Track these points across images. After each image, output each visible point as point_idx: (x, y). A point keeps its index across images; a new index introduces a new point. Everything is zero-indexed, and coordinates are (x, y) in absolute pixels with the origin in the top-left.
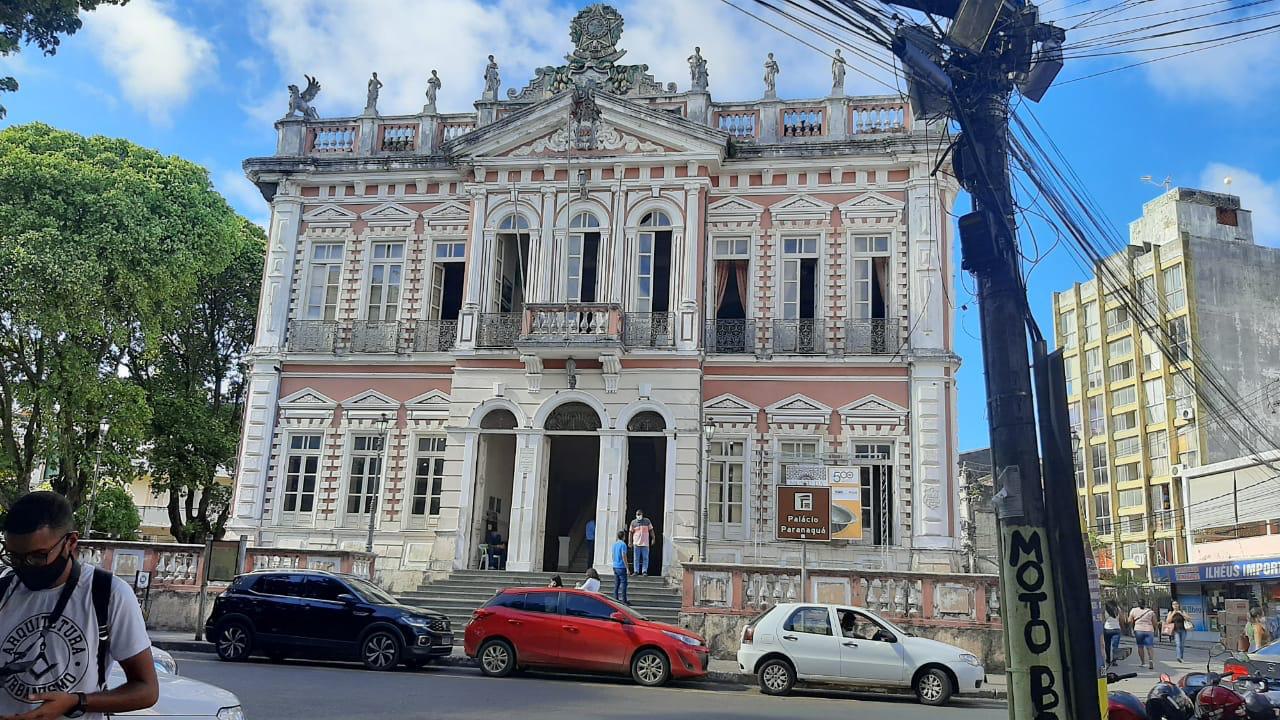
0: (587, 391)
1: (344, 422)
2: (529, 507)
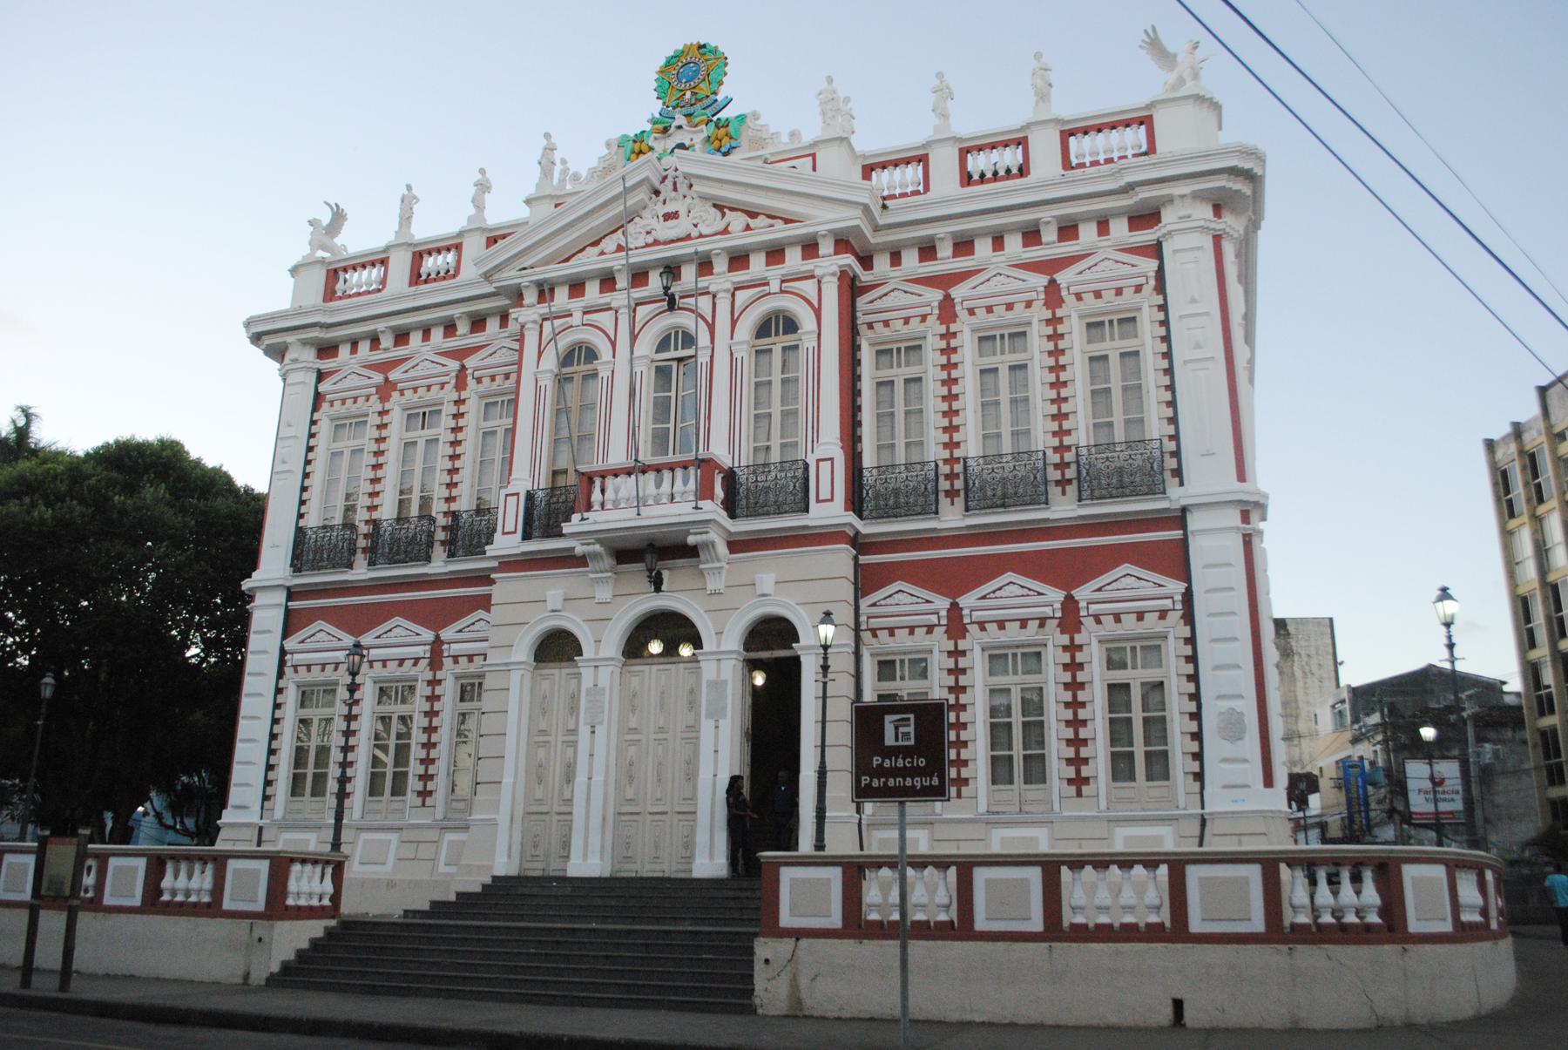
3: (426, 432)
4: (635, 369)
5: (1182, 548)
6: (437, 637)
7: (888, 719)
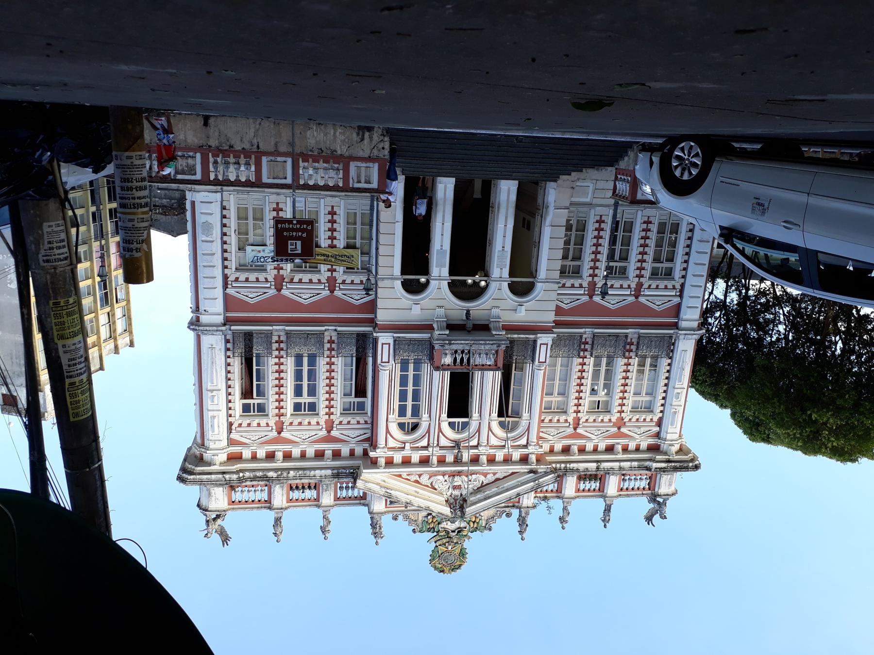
0: (456, 307)
1: (633, 286)
2: (500, 226)
3: (597, 399)
4: (478, 415)
5: (227, 308)
7: (299, 252)
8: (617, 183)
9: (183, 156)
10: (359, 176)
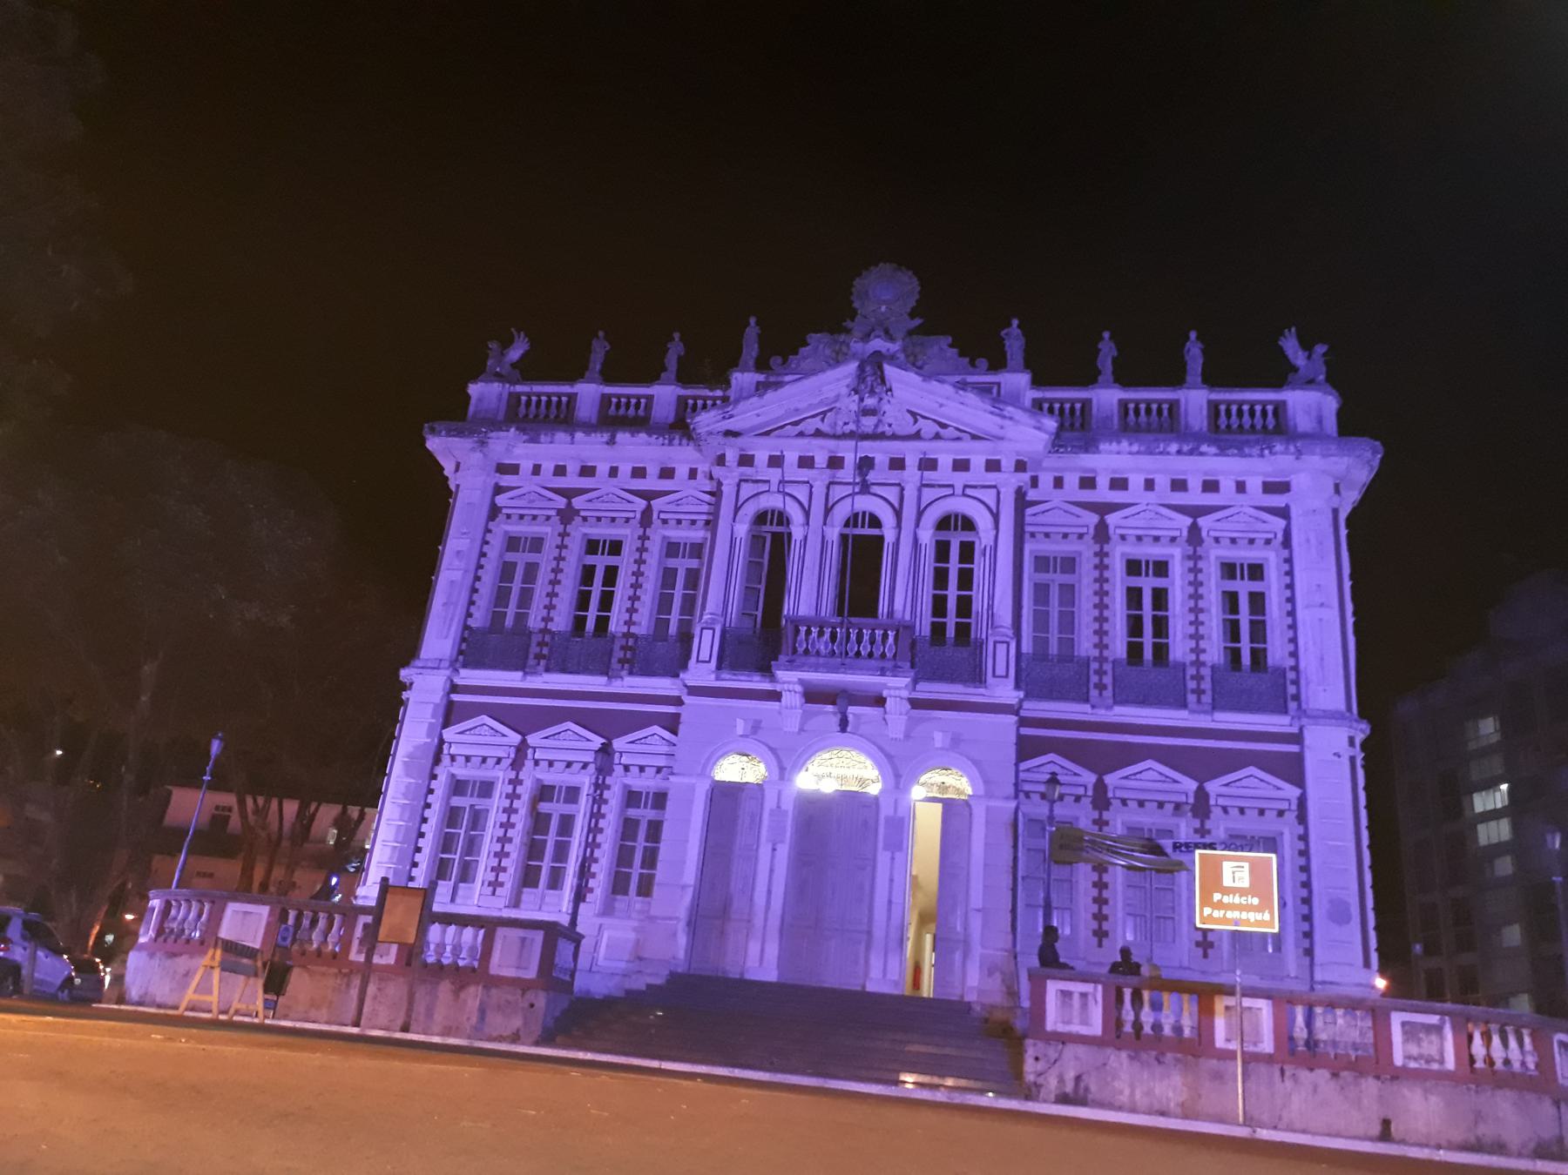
5: (1299, 759)
6: (524, 741)
8: (572, 965)
9: (1428, 1062)
10: (1084, 1006)
